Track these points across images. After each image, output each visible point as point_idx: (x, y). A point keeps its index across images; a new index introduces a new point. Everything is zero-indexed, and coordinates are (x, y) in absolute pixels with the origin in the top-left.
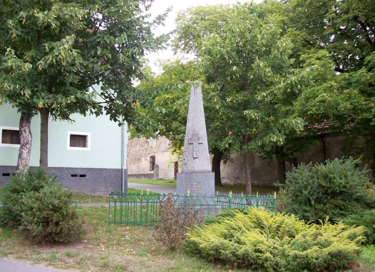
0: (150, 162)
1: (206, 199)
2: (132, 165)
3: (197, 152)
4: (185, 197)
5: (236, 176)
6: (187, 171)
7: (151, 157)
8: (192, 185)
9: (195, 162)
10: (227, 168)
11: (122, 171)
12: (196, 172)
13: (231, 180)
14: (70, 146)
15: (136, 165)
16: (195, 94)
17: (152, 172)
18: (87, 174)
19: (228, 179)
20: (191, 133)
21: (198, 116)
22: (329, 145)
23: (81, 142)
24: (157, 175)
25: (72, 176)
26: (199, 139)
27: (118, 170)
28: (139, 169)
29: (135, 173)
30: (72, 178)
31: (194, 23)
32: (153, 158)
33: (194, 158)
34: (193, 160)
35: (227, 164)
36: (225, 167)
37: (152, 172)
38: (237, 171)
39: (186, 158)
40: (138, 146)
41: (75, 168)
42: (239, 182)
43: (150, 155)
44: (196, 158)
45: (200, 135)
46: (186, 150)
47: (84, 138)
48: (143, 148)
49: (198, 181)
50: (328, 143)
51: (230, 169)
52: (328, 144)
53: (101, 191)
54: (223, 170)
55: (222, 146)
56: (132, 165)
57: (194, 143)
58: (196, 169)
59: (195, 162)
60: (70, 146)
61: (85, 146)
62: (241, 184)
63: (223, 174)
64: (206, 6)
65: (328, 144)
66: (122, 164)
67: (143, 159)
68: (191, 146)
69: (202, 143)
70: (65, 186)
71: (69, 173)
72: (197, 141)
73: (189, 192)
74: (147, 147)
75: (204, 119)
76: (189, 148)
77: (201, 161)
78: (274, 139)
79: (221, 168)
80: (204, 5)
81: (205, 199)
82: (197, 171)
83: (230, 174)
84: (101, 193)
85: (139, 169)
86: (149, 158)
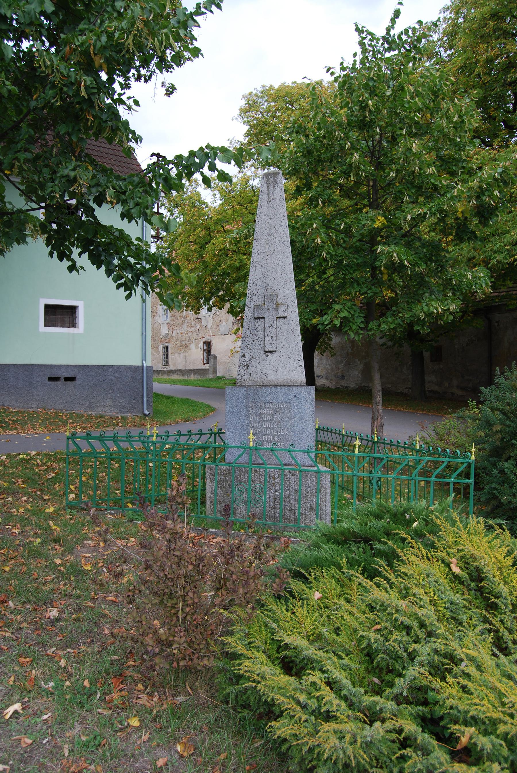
0: (204, 350)
1: (294, 455)
2: (176, 355)
3: (274, 338)
4: (242, 450)
5: (340, 374)
6: (251, 383)
7: (204, 343)
8: (261, 416)
9: (268, 362)
10: (324, 361)
11: (143, 370)
12: (271, 386)
13: (331, 380)
14: (45, 326)
15: (182, 355)
16: (268, 202)
17: (207, 366)
18: (78, 376)
19: (327, 379)
20: (261, 291)
21: (276, 252)
22: (498, 325)
23: (67, 319)
24: (215, 371)
25: (51, 379)
26: (278, 307)
27: (136, 368)
28: (186, 361)
29: (179, 368)
30: (50, 383)
31: (274, 117)
32: (208, 344)
33: (266, 352)
34: (263, 355)
35: (325, 354)
36: (321, 359)
37: (207, 366)
38: (341, 366)
39: (249, 351)
40: (185, 326)
41: (55, 366)
42: (344, 384)
43: (204, 340)
44: (271, 352)
45: (281, 297)
46: (248, 333)
47: (72, 310)
48: (192, 329)
49: (277, 405)
50: (497, 322)
51: (330, 363)
52: (496, 324)
53: (104, 406)
54: (319, 364)
55: (326, 323)
56: (176, 355)
57: (266, 316)
58: (272, 377)
59: (268, 362)
60: (45, 326)
61: (73, 324)
62: (346, 387)
63: (318, 371)
64: (293, 85)
65: (496, 324)
66: (142, 357)
67: (193, 346)
68: (260, 325)
69: (284, 318)
70: (38, 398)
71: (44, 374)
72: (273, 313)
73: (251, 436)
74: (198, 327)
75: (291, 260)
76: (255, 329)
77: (282, 360)
78: (437, 308)
79: (316, 361)
80: (289, 82)
81: (291, 455)
82: (272, 383)
83: (329, 371)
84: (106, 409)
85: (186, 361)
86: (201, 345)
